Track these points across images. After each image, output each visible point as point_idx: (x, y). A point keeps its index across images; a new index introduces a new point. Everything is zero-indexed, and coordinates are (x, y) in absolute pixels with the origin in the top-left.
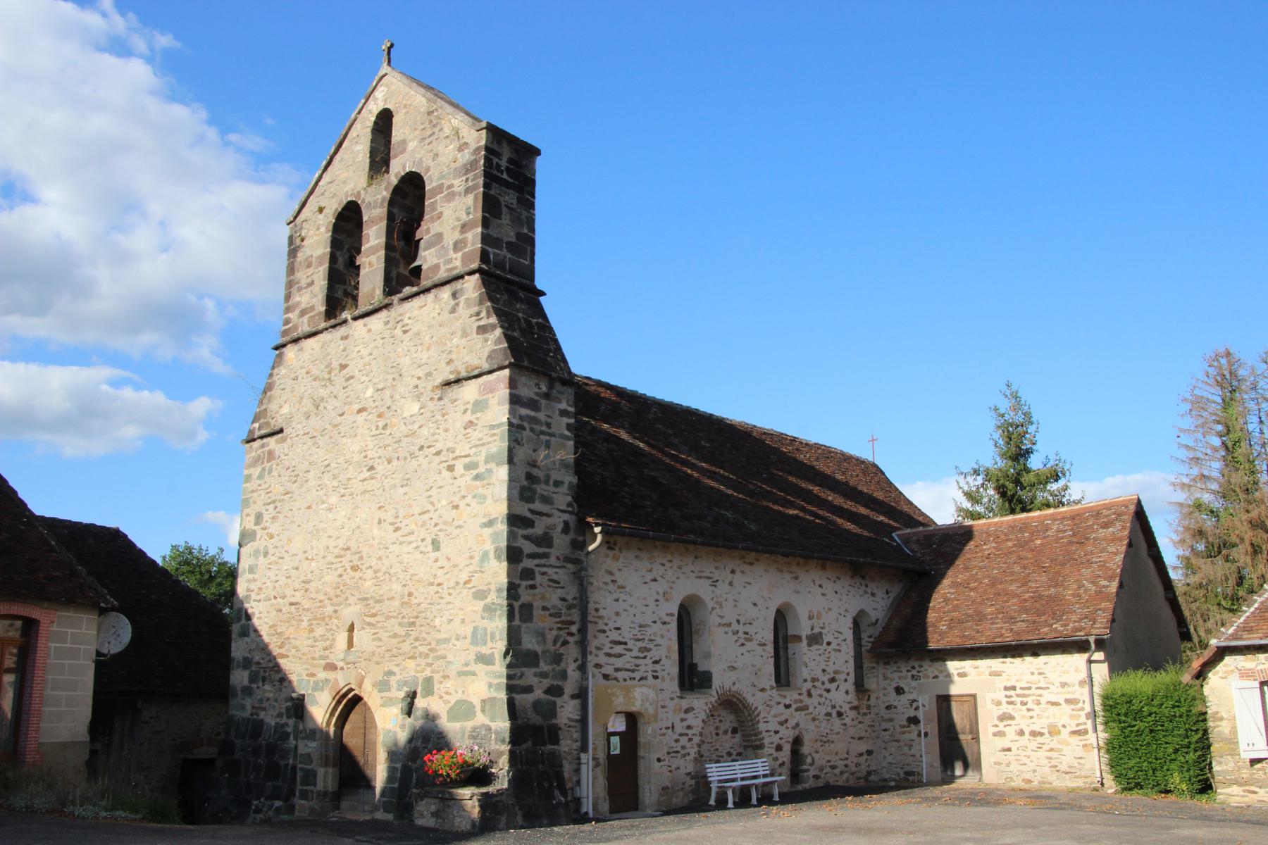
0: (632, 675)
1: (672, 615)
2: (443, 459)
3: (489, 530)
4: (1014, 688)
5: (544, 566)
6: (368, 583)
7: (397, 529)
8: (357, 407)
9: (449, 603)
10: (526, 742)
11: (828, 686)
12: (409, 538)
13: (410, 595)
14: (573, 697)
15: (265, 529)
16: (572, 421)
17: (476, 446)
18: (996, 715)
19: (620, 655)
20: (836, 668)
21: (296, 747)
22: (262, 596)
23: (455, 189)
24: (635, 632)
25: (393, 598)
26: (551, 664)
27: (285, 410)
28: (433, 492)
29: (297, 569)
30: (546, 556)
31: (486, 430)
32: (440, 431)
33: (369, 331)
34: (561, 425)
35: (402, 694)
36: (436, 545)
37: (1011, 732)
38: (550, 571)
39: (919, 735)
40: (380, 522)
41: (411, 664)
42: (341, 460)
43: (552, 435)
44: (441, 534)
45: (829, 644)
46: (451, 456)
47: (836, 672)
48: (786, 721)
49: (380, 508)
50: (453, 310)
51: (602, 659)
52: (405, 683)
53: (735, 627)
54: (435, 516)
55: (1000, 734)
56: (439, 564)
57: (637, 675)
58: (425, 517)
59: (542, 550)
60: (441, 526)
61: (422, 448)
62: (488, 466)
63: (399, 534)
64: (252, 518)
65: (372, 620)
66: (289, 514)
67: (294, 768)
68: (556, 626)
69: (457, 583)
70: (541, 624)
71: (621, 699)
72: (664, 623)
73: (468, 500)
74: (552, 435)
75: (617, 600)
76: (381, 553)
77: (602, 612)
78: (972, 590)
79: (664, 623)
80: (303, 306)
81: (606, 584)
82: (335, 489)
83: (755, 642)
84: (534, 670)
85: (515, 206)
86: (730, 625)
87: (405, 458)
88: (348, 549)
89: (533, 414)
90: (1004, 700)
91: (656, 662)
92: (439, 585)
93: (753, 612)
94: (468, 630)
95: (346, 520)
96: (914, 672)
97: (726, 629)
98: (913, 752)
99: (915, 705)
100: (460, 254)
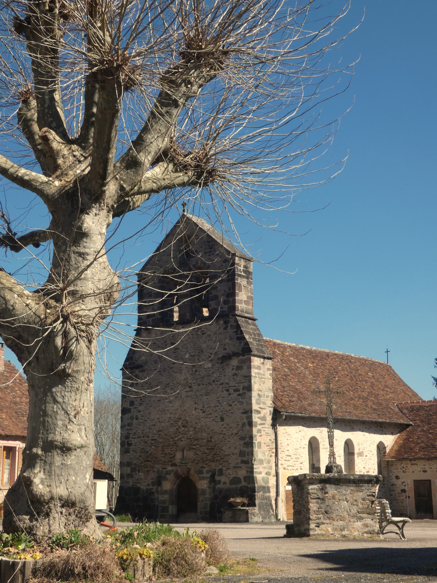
1: (306, 445)
2: (224, 386)
3: (246, 415)
5: (264, 428)
6: (191, 433)
7: (204, 412)
9: (229, 441)
12: (210, 416)
13: (211, 437)
14: (274, 476)
15: (136, 408)
19: (289, 461)
21: (158, 497)
22: (136, 436)
25: (203, 439)
26: (267, 464)
29: (155, 425)
31: (242, 377)
32: (222, 376)
35: (208, 475)
36: (222, 419)
38: (266, 429)
39: (406, 497)
40: (196, 409)
41: (213, 464)
42: (175, 382)
43: (265, 378)
45: (366, 456)
46: (227, 386)
47: (369, 469)
49: (195, 403)
50: (225, 328)
51: (283, 462)
52: (210, 471)
56: (223, 426)
57: (295, 468)
58: (217, 408)
59: (263, 422)
61: (214, 381)
62: (244, 391)
63: (205, 414)
64: (128, 403)
65: (194, 447)
67: (157, 506)
69: (232, 434)
70: (264, 449)
72: (304, 448)
73: (236, 403)
74: (265, 378)
75: (287, 440)
78: (430, 433)
79: (304, 448)
81: (284, 433)
84: (262, 466)
85: (246, 285)
87: (206, 385)
88: (181, 418)
89: (259, 371)
91: (301, 463)
92: (224, 434)
94: (237, 451)
95: (179, 407)
96: (404, 469)
98: (403, 505)
99: (404, 484)
100: (226, 306)
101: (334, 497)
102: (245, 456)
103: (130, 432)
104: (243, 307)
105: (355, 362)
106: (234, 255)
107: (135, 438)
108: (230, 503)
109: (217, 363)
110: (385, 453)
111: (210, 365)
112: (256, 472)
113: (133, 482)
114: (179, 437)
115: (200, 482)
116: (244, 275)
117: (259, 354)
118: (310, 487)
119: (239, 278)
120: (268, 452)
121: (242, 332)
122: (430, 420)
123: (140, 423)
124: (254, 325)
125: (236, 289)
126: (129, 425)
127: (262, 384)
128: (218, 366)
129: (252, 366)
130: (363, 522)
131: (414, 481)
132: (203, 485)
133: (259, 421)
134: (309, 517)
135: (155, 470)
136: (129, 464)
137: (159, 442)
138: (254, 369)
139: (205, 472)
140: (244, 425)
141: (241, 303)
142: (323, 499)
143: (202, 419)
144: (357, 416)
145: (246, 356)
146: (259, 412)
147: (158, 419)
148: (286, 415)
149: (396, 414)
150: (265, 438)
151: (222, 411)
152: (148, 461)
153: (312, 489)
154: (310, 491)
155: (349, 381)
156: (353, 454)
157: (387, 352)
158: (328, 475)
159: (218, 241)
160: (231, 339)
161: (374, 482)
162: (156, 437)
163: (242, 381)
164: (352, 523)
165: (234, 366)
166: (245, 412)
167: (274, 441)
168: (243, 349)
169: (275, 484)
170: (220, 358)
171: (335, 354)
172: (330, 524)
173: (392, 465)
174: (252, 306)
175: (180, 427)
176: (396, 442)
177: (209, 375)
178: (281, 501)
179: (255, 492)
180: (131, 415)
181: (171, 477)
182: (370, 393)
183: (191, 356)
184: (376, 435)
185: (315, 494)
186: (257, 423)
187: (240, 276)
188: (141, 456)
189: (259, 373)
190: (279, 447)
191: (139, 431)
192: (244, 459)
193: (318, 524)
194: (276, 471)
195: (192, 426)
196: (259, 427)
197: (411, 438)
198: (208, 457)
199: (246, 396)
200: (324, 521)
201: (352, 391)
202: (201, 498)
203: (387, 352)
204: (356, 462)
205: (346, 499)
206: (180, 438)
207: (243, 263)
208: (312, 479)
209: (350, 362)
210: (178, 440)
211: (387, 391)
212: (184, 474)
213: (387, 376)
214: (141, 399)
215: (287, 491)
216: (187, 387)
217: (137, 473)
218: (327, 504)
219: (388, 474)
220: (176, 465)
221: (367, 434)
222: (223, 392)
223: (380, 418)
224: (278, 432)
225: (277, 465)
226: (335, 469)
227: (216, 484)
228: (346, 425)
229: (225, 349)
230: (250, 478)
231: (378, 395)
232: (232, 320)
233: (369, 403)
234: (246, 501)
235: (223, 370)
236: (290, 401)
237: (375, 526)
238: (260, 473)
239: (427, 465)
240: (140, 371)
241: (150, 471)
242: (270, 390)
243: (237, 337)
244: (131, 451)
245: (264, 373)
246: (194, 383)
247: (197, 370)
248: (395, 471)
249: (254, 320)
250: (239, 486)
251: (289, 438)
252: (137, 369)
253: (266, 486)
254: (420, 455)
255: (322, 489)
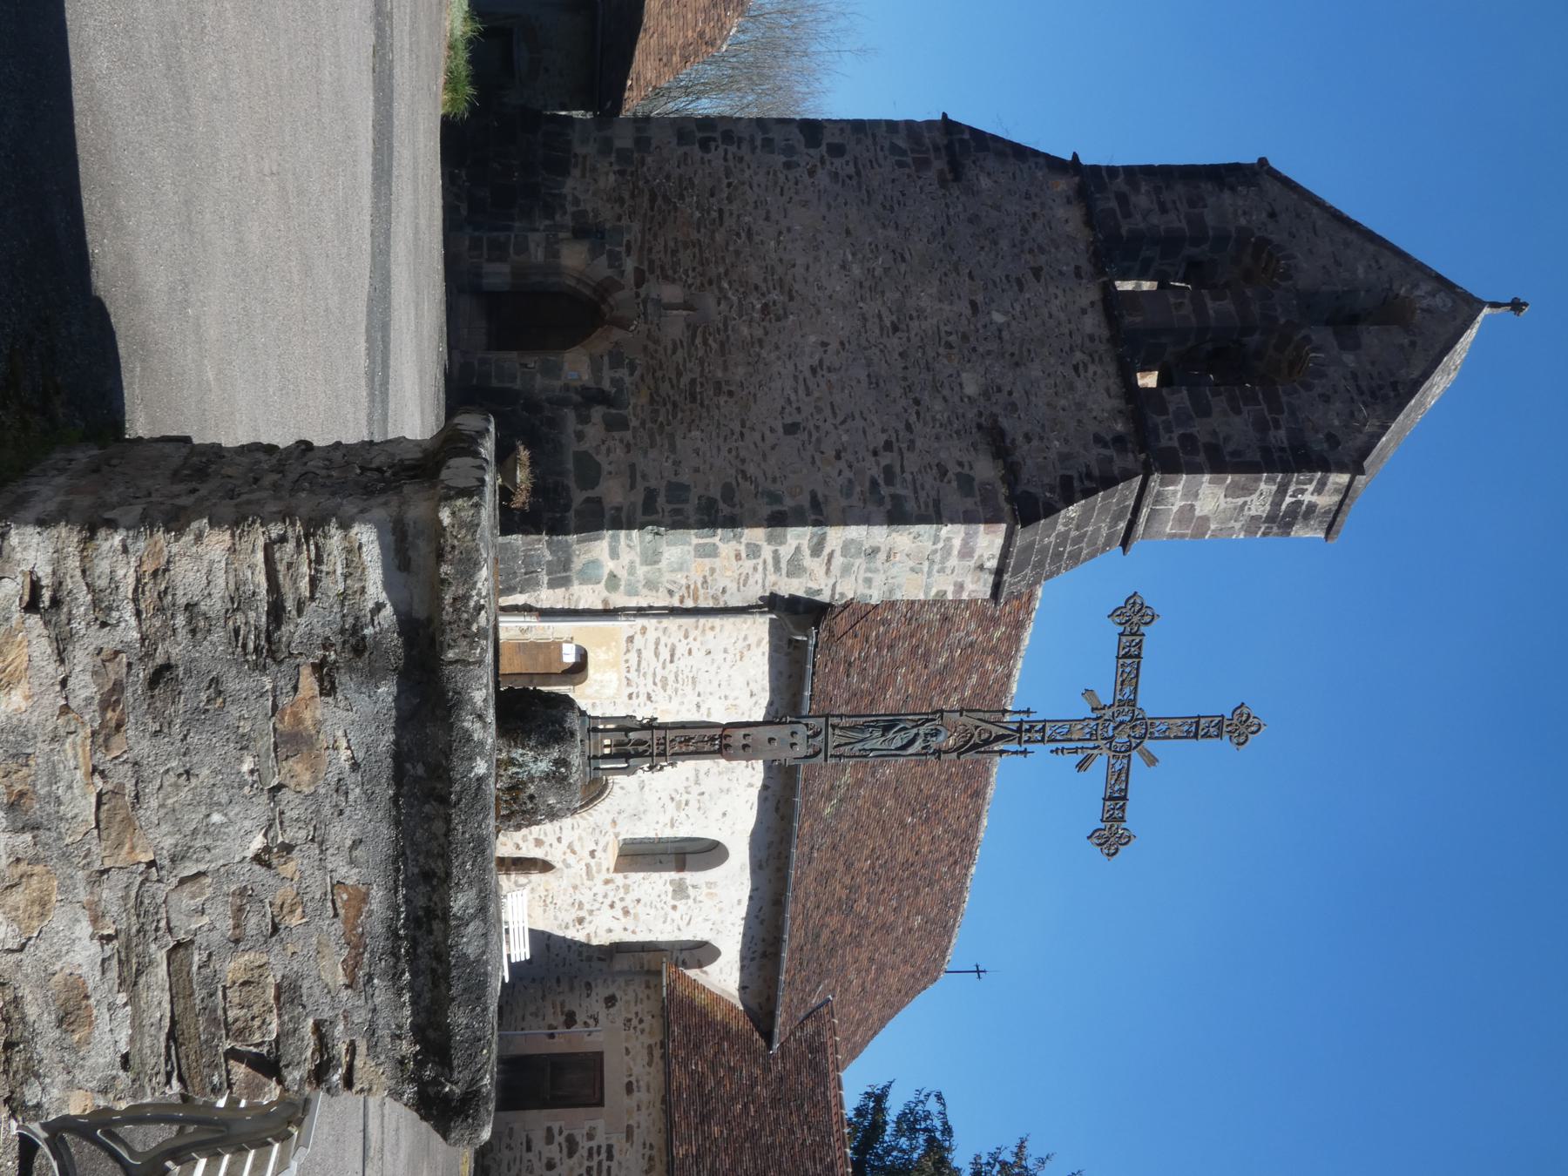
0: (633, 669)
1: (709, 715)
2: (901, 434)
3: (807, 505)
4: (610, 1157)
6: (745, 331)
7: (813, 370)
8: (979, 298)
10: (552, 553)
11: (619, 905)
13: (731, 394)
14: (605, 601)
15: (823, 162)
16: (950, 597)
17: (914, 481)
18: (575, 1132)
19: (657, 655)
20: (643, 917)
23: (1272, 432)
24: (686, 672)
25: (725, 369)
27: (985, 183)
28: (859, 423)
30: (777, 568)
31: (933, 494)
33: (1084, 312)
34: (943, 585)
35: (606, 385)
36: (791, 429)
37: (552, 1151)
38: (759, 576)
39: (551, 1027)
40: (824, 344)
41: (644, 399)
43: (930, 574)
44: (805, 436)
45: (674, 908)
46: (904, 446)
47: (636, 917)
48: (574, 852)
49: (842, 344)
50: (1098, 439)
51: (652, 635)
52: (620, 391)
53: (695, 790)
54: (828, 426)
55: (550, 1139)
56: (768, 433)
57: (633, 675)
58: (828, 412)
59: (784, 565)
60: (815, 435)
61: (917, 402)
63: (808, 374)
64: (837, 140)
65: (698, 341)
66: (841, 200)
67: (509, 228)
68: (691, 583)
69: (743, 461)
71: (603, 657)
72: (698, 706)
73: (847, 474)
74: (930, 574)
75: (725, 651)
76: (784, 348)
77: (710, 634)
78: (745, 1106)
79: (698, 706)
80: (1133, 199)
81: (745, 638)
82: (871, 271)
83: (675, 814)
84: (638, 560)
85: (1246, 512)
86: (697, 783)
87: (905, 379)
88: (791, 299)
89: (955, 552)
90: (594, 1144)
91: (649, 697)
92: (742, 434)
93: (716, 813)
94: (685, 477)
95: (827, 293)
96: (635, 1022)
97: (692, 779)
98: (528, 1017)
99: (591, 1022)
100: (1176, 444)
101: (293, 742)
102: (668, 502)
103: (745, 147)
104: (1172, 500)
105: (953, 877)
106: (1357, 469)
107: (725, 160)
108: (514, 449)
109: (980, 414)
110: (685, 965)
111: (971, 389)
112: (615, 539)
113: (585, 157)
114: (730, 294)
115: (586, 359)
116: (1284, 507)
117: (1014, 551)
118: (366, 536)
119: (1274, 488)
120: (684, 582)
121: (1088, 493)
122: (787, 1106)
123: (775, 174)
124: (1108, 542)
125: (1237, 477)
126: (768, 143)
127: (911, 563)
128: (970, 415)
129: (974, 526)
130: (103, 989)
131: (601, 1054)
132: (576, 367)
133: (786, 551)
134: (113, 525)
135: (625, 222)
136: (642, 143)
137: (713, 232)
138: (962, 535)
139: (617, 375)
140: (775, 498)
141: (1185, 496)
142: (269, 651)
143: (790, 366)
144: (799, 881)
145: (1007, 507)
146: (817, 550)
147: (789, 230)
148: (805, 643)
149: (803, 1000)
150: (729, 573)
151: (817, 428)
152: (653, 199)
153: (353, 552)
154: (335, 541)
155: (900, 858)
156: (681, 867)
157: (978, 971)
158: (481, 695)
159: (1401, 417)
160: (1064, 458)
161: (434, 1081)
162: (729, 222)
163: (923, 495)
164: (83, 895)
165: (971, 468)
166: (816, 504)
167: (722, 605)
168: (1029, 496)
169: (581, 607)
170: (996, 421)
171: (978, 817)
172: (66, 709)
173: (648, 987)
174: (1174, 536)
175: (763, 295)
176: (718, 999)
177: (936, 388)
178: (525, 625)
179: (551, 532)
180: (802, 148)
181: (602, 268)
182: (863, 922)
183: (1000, 331)
184: (740, 938)
185: (314, 582)
186: (781, 543)
187: (1282, 490)
188: (668, 178)
189: (949, 554)
190: (703, 621)
191: (748, 173)
192: (661, 500)
193: (56, 602)
194: (624, 609)
195: (766, 333)
196: (767, 551)
197: (731, 1046)
198: (667, 384)
199: (871, 508)
200: (81, 657)
201: (872, 866)
202: (533, 362)
203: (978, 971)
204: (655, 876)
205: (288, 848)
206: (726, 298)
207: (1326, 501)
208: (440, 556)
209: (956, 863)
210: (721, 289)
211: (868, 971)
212: (612, 308)
213: (910, 970)
214: (850, 178)
215: (557, 646)
216: (894, 318)
217: (616, 168)
218: (231, 685)
219: (621, 973)
220: (639, 284)
221: (742, 910)
222: (884, 431)
223: (792, 952)
224: (749, 619)
225: (641, 612)
226: (544, 765)
227: (576, 407)
228: (770, 845)
229: (1028, 438)
230: (596, 520)
231: (859, 945)
232: (1129, 461)
233: (835, 919)
234: (520, 500)
235: (958, 432)
236: (850, 664)
237: (70, 1085)
238: (614, 554)
239: (648, 1096)
240: (941, 172)
241: (622, 206)
242: (891, 591)
243: (1070, 478)
244: (686, 148)
245: (948, 571)
246: (909, 340)
247: (951, 347)
248: (631, 996)
249: (1125, 543)
250: (571, 483)
251: (730, 657)
252: (949, 163)
253: (573, 574)
254: (680, 1077)
255: (356, 643)
